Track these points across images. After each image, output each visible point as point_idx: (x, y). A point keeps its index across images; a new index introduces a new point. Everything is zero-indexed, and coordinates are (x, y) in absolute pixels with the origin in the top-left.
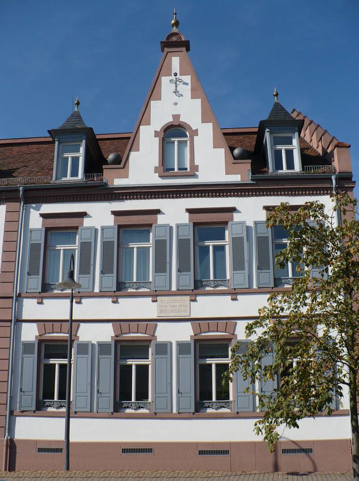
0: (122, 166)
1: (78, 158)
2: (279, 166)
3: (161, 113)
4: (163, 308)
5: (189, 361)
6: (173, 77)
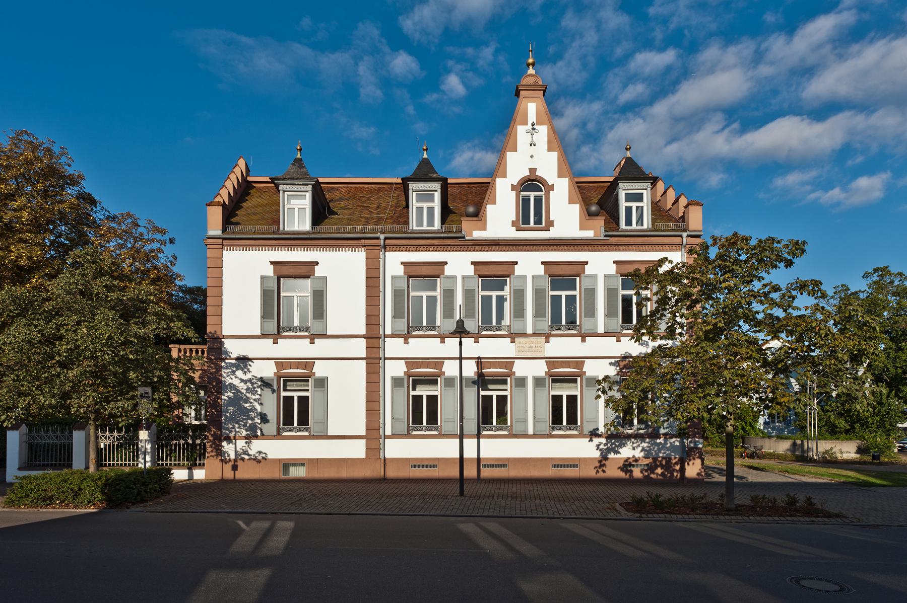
3: (517, 166)
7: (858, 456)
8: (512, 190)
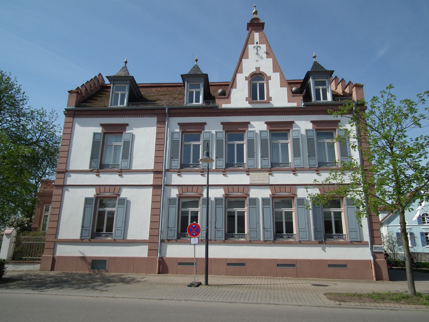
0: (227, 96)
1: (124, 94)
2: (318, 98)
3: (249, 67)
4: (253, 178)
5: (269, 211)
6: (255, 45)
7: (213, 199)
8: (246, 80)
